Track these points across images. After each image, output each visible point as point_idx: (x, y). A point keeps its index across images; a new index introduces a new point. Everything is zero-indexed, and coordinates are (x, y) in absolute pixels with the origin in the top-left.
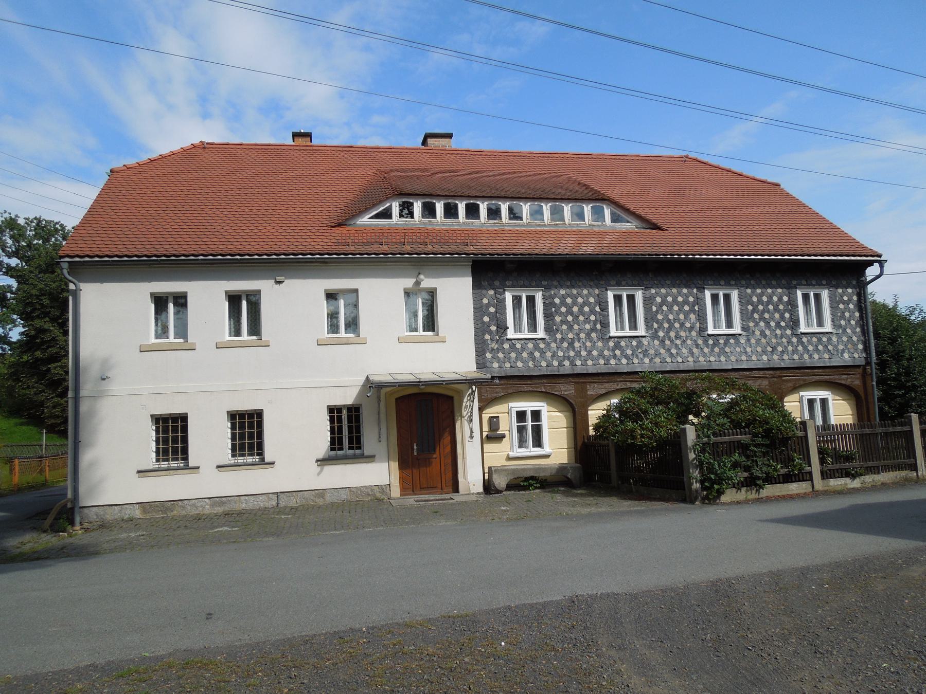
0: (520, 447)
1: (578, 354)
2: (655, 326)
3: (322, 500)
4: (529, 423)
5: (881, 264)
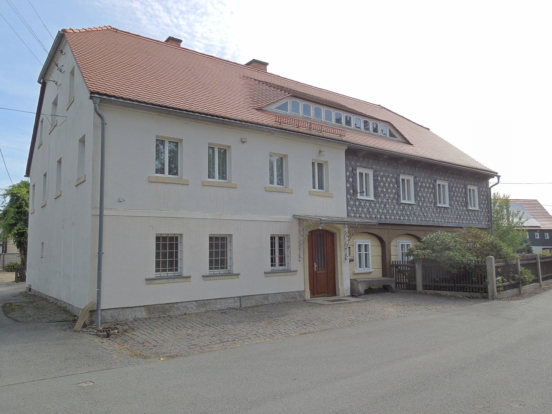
0: (281, 265)
1: (388, 212)
2: (419, 199)
3: (266, 301)
4: (363, 252)
5: (499, 177)
